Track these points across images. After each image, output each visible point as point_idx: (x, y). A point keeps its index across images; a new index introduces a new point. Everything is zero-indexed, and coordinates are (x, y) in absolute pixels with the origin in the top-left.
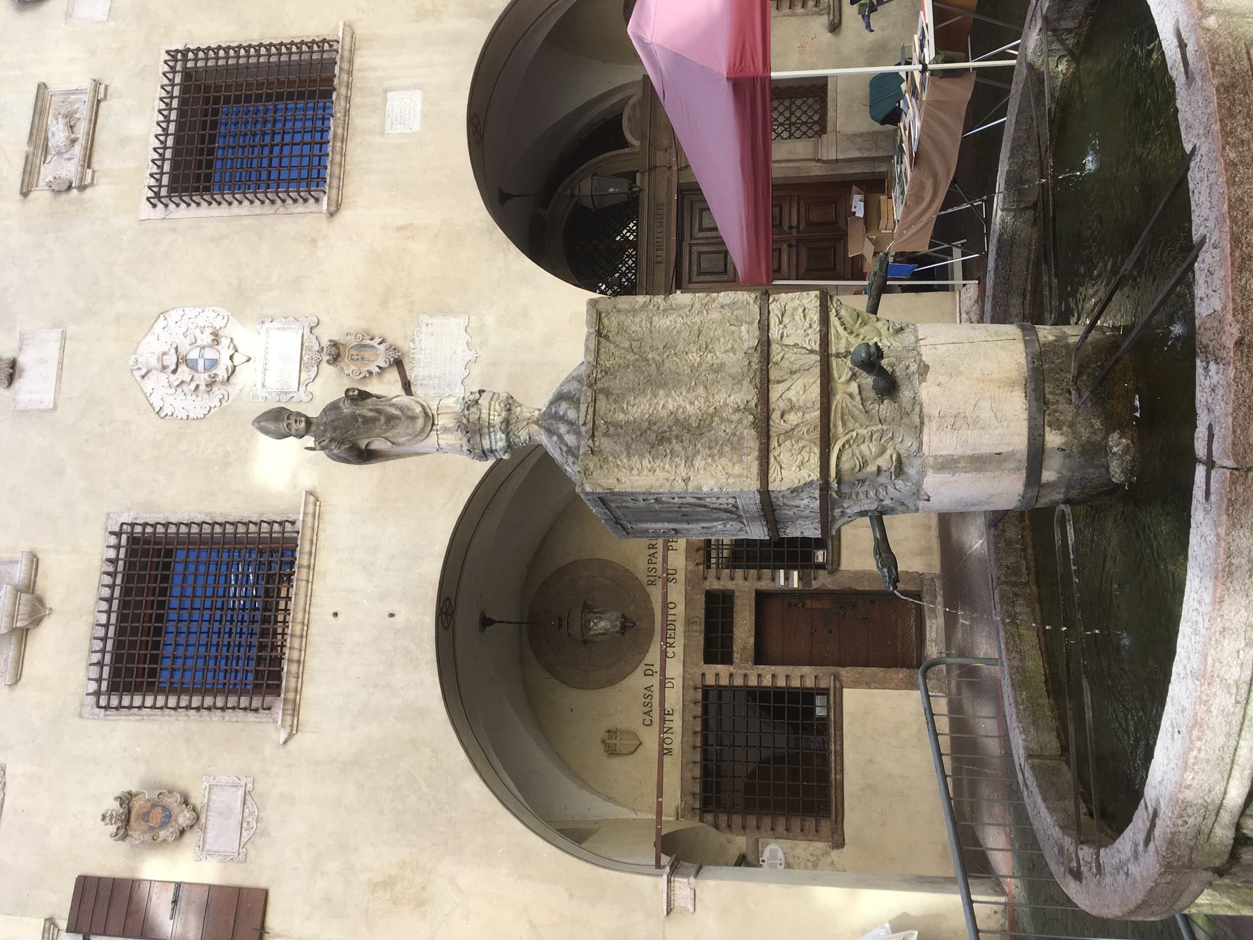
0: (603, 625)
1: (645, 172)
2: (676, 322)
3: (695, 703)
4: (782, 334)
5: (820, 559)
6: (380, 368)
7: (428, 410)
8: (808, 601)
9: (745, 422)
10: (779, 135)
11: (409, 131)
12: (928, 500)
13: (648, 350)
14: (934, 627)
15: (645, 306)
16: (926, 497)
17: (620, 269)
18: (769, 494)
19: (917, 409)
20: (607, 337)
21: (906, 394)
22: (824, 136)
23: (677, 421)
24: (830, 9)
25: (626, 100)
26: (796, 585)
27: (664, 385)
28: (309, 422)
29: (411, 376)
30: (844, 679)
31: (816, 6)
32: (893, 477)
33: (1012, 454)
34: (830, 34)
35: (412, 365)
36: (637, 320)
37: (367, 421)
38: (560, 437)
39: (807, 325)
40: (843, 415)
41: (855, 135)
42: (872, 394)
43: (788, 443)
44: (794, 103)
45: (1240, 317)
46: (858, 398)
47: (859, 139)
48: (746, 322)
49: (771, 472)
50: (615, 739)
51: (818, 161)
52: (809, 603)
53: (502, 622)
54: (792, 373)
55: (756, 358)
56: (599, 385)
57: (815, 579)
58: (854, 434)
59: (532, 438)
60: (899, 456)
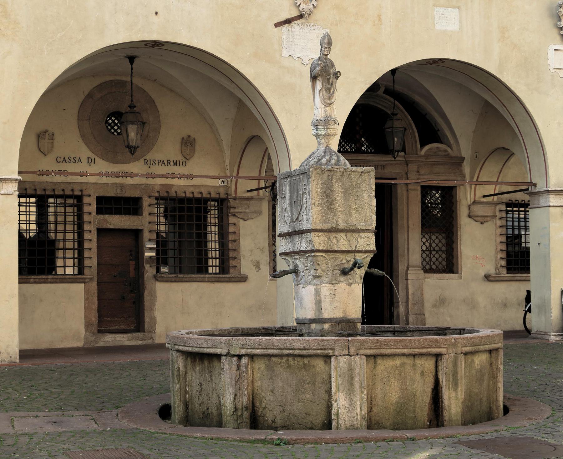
0: (132, 135)
1: (405, 158)
2: (366, 200)
3: (72, 190)
4: (362, 237)
5: (163, 270)
6: (299, 5)
7: (332, 104)
8: (134, 263)
9: (333, 224)
10: (424, 244)
11: (435, 22)
12: (303, 288)
13: (357, 190)
14: (123, 339)
15: (372, 188)
16: (304, 287)
17: (348, 145)
18: (309, 232)
19: (337, 282)
20: (361, 175)
21: (342, 278)
22: (422, 271)
23: (333, 200)
24: (499, 274)
25: (450, 146)
26: (146, 254)
27: (345, 196)
28: (327, 55)
29: (295, 24)
30: (90, 284)
31: (501, 266)
32: (313, 275)
33: (322, 313)
34: (483, 275)
35: (300, 24)
36: (367, 186)
37: (328, 80)
38: (324, 157)
39: (365, 246)
40: (335, 258)
41: (422, 290)
42: (342, 267)
43: (326, 239)
44: (443, 253)
45: (384, 341)
46: (341, 263)
47: (419, 292)
48: (366, 225)
49: (317, 233)
50: (48, 139)
51: (408, 268)
52: (132, 263)
53: (132, 69)
54: (349, 241)
55: (354, 228)
56: (345, 172)
57: (151, 266)
58: (329, 261)
59: (321, 144)
60: (321, 276)
